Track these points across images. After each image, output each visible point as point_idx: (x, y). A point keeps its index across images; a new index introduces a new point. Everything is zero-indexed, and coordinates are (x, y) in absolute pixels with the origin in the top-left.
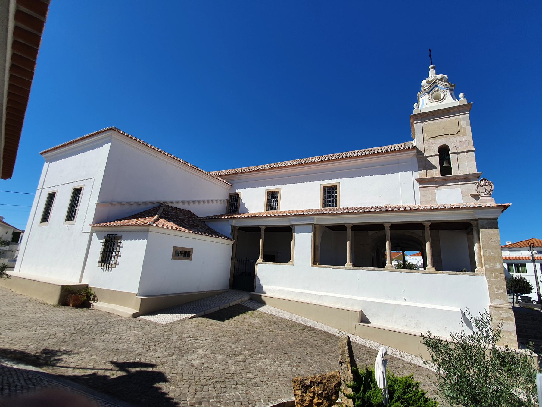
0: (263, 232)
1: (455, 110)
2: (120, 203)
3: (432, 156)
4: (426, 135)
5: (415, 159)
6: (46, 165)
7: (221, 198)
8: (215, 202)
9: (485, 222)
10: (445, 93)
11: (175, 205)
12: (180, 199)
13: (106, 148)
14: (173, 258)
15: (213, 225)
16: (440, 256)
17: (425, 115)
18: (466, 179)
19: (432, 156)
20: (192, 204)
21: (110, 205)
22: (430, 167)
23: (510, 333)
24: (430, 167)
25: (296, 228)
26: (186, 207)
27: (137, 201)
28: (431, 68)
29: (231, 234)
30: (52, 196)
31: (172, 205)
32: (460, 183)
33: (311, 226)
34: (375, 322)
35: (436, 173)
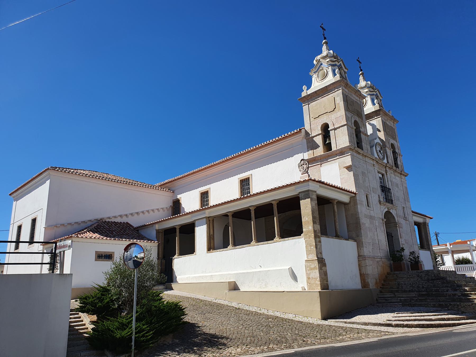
0: (178, 231)
1: (331, 88)
2: (63, 225)
3: (316, 136)
4: (311, 116)
5: (305, 141)
6: (14, 203)
7: (166, 206)
8: (156, 211)
9: (303, 194)
10: (328, 70)
11: (113, 220)
12: (117, 214)
13: (47, 185)
14: (96, 260)
15: (143, 232)
16: (326, 228)
17: (331, 88)
18: (342, 152)
19: (316, 136)
20: (130, 216)
21: (55, 228)
22: (313, 146)
23: (316, 279)
24: (313, 146)
25: (197, 223)
26: (124, 220)
27: (77, 221)
28: (324, 43)
29: (157, 238)
30: (20, 228)
31: (110, 220)
32: (338, 157)
33: (205, 219)
34: (242, 289)
35: (320, 151)
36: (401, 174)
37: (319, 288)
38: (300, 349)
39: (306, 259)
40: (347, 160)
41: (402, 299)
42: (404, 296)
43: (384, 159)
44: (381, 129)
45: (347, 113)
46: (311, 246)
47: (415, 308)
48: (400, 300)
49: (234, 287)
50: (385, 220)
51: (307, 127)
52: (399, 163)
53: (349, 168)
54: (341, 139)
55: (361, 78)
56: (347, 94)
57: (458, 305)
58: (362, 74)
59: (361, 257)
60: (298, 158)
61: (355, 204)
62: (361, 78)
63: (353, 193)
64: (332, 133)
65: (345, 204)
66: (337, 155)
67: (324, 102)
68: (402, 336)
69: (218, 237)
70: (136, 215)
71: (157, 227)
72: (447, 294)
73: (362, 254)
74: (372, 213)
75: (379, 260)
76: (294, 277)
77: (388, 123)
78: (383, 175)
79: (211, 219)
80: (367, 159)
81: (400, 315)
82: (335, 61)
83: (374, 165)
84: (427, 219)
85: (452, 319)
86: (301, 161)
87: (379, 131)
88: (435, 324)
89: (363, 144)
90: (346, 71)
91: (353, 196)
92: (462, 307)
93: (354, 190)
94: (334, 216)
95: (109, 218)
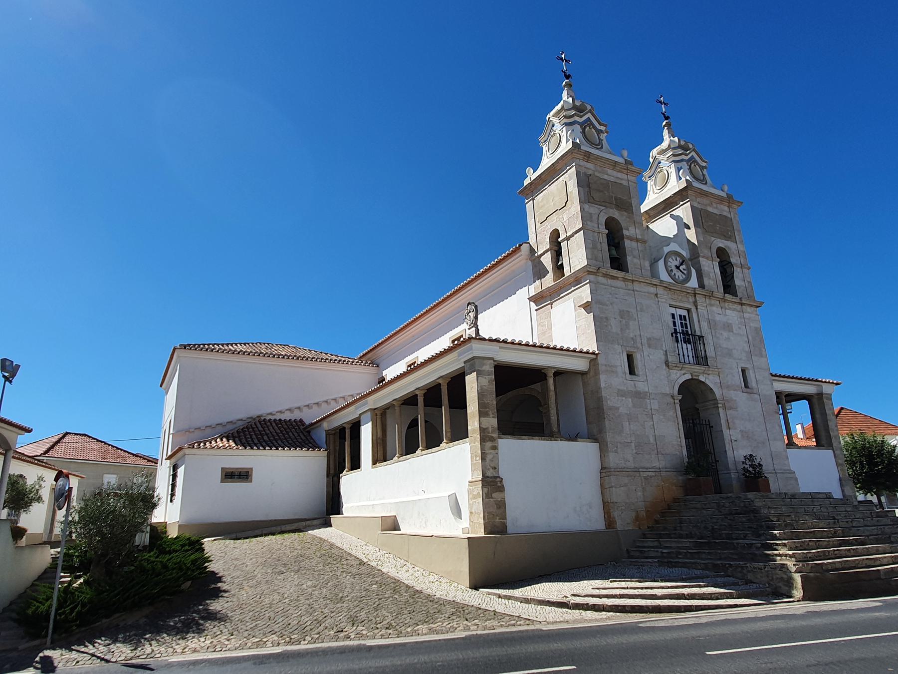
20: (305, 409)
26: (296, 416)
31: (273, 418)
34: (405, 529)
36: (742, 304)
37: (483, 530)
38: (290, 648)
39: (470, 479)
40: (584, 293)
41: (665, 551)
42: (673, 545)
43: (688, 278)
44: (691, 223)
45: (586, 206)
46: (476, 456)
47: (676, 571)
48: (662, 553)
49: (392, 525)
50: (680, 397)
51: (532, 240)
52: (738, 282)
53: (587, 307)
54: (576, 257)
55: (666, 132)
56: (590, 172)
57: (742, 567)
58: (668, 125)
59: (605, 470)
60: (524, 293)
61: (597, 373)
62: (666, 132)
63: (593, 353)
64: (564, 245)
65: (583, 374)
66: (571, 285)
67: (552, 194)
68: (527, 631)
69: (396, 438)
70: (315, 407)
71: (326, 425)
72: (738, 543)
73: (606, 465)
74: (642, 386)
75: (653, 474)
76: (457, 511)
77: (710, 209)
78: (689, 311)
79: (379, 413)
80: (637, 286)
81: (615, 585)
82: (572, 116)
83: (656, 295)
84: (825, 386)
85: (710, 597)
86: (469, 304)
87: (689, 228)
88: (647, 607)
89: (629, 258)
90: (603, 128)
91: (593, 358)
92: (749, 572)
93: (593, 347)
94: (527, 397)
95: (271, 414)
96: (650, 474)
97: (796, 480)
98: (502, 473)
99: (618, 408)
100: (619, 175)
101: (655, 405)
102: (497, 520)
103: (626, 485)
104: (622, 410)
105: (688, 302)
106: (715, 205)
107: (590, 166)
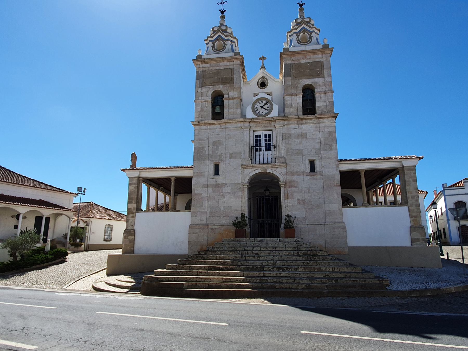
77: (303, 61)
96: (215, 227)
97: (345, 228)
98: (136, 228)
99: (201, 194)
100: (228, 64)
101: (229, 190)
102: (129, 248)
103: (197, 233)
104: (205, 195)
105: (271, 126)
106: (308, 57)
107: (208, 65)
